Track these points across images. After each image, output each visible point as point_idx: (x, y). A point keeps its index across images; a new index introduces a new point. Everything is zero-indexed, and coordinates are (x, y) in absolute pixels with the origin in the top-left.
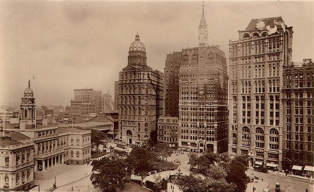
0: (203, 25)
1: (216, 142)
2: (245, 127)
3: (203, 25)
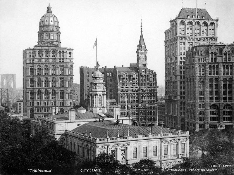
0: (49, 5)
3: (49, 5)
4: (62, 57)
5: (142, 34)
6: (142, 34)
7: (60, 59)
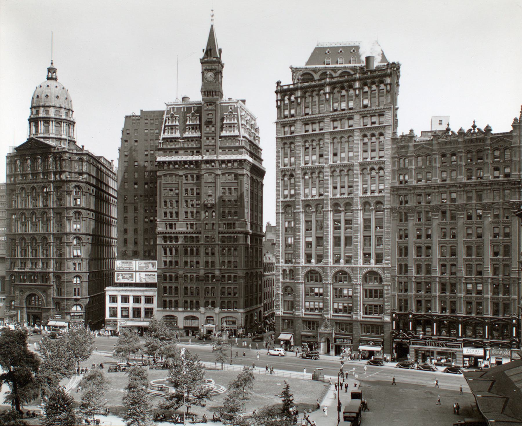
1: (242, 311)
2: (372, 273)
3: (52, 64)
4: (59, 170)
5: (339, 401)
6: (339, 401)
7: (55, 173)
